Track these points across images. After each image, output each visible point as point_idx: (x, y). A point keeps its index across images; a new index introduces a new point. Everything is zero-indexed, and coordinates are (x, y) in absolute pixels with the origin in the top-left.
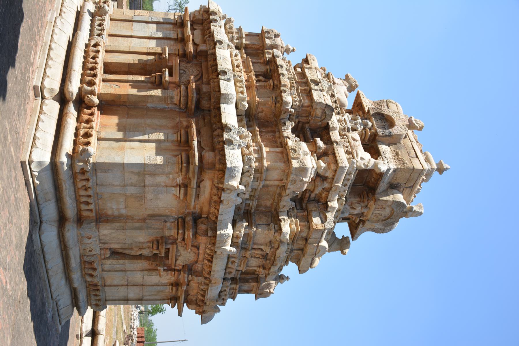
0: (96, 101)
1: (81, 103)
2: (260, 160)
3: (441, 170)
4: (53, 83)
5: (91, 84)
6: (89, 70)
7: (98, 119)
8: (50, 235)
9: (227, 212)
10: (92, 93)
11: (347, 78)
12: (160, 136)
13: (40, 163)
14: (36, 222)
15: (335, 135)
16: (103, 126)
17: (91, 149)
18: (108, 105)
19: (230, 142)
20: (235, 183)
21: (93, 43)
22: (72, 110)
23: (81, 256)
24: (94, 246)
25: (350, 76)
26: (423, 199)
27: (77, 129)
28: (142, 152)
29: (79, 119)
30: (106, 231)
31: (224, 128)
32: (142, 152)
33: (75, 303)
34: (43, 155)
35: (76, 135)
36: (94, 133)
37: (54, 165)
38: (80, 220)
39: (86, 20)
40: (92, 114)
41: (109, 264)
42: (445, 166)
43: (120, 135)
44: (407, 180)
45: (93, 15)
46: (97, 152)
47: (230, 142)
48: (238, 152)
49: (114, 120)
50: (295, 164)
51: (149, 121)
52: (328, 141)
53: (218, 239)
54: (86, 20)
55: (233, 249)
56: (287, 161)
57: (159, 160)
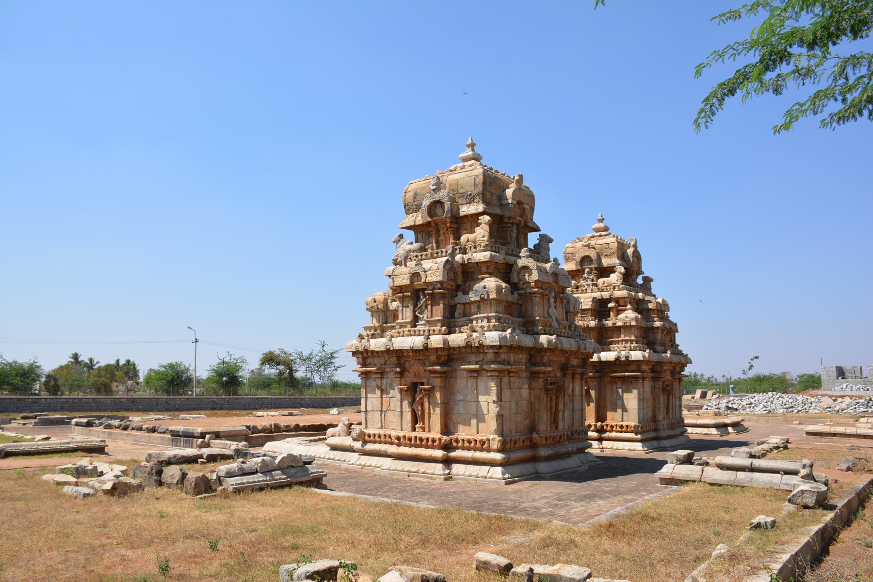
0: (599, 424)
1: (601, 431)
2: (632, 342)
3: (472, 146)
4: (439, 468)
5: (434, 441)
6: (422, 443)
7: (609, 422)
8: (543, 467)
9: (527, 341)
10: (596, 425)
11: (397, 242)
12: (620, 391)
13: (503, 474)
14: (538, 476)
15: (606, 295)
16: (613, 420)
17: (633, 424)
18: (446, 430)
19: (627, 357)
20: (647, 355)
21: (397, 441)
22: (607, 435)
23: (669, 429)
24: (665, 423)
25: (393, 239)
26: (507, 168)
27: (617, 432)
28: (631, 400)
29: (611, 431)
30: (661, 417)
31: (618, 359)
32: (631, 400)
33: (581, 450)
34: (497, 472)
35: (621, 432)
36: (620, 423)
37: (502, 464)
38: (656, 430)
39: (370, 447)
40: (607, 425)
41: (560, 427)
42: (470, 142)
43: (619, 411)
44: (491, 186)
45: (365, 442)
46: (632, 420)
47: (627, 357)
48: (632, 353)
49: (609, 414)
50: (633, 323)
51: (608, 397)
52: (609, 300)
53: (503, 344)
54: (370, 447)
55: (669, 352)
56: (631, 327)
57: (635, 392)
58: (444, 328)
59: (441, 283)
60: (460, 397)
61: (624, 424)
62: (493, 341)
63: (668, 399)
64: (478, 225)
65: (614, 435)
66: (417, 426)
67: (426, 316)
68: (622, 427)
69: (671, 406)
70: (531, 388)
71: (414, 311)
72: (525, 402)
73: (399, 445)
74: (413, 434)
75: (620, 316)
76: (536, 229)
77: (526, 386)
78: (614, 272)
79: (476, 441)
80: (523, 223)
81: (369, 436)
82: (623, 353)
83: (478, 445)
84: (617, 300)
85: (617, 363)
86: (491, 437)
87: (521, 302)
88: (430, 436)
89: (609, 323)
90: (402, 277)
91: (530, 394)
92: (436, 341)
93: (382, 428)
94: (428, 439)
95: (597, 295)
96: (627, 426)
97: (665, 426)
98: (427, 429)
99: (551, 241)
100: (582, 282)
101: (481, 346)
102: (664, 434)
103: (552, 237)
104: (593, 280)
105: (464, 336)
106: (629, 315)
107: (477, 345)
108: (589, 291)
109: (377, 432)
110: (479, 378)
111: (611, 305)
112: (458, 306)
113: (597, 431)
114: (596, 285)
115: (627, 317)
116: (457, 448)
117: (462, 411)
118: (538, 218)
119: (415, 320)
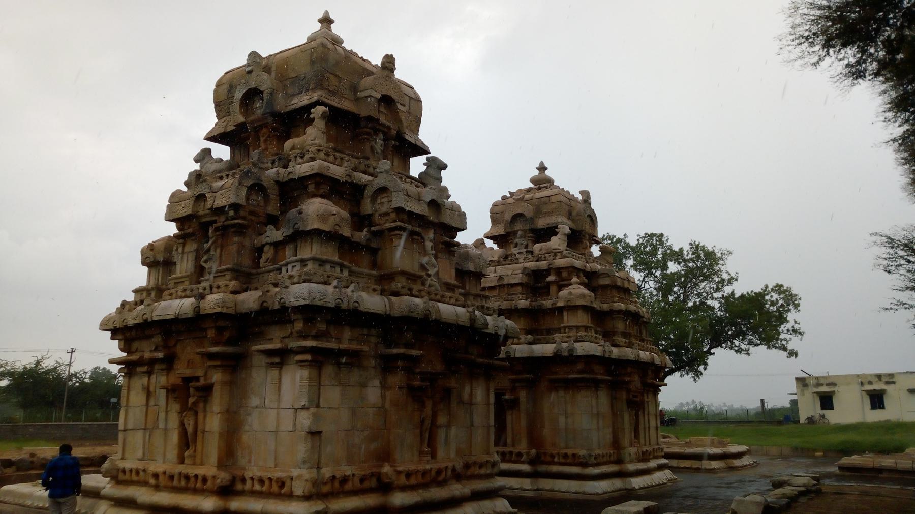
0: (534, 451)
15: (543, 265)
21: (152, 481)
41: (441, 453)
48: (577, 345)
52: (548, 272)
58: (234, 282)
59: (235, 207)
60: (254, 401)
61: (570, 452)
62: (299, 299)
63: (637, 416)
64: (311, 121)
65: (555, 468)
66: (186, 454)
67: (214, 266)
68: (566, 456)
69: (641, 427)
70: (384, 387)
71: (197, 259)
72: (371, 411)
73: (157, 488)
74: (181, 468)
75: (561, 293)
76: (421, 150)
77: (377, 383)
78: (556, 234)
79: (270, 479)
80: (394, 132)
81: (124, 471)
82: (565, 345)
83: (275, 488)
84: (558, 271)
85: (557, 358)
86: (295, 473)
87: (374, 245)
88: (201, 471)
89: (547, 303)
90: (183, 204)
91: (383, 397)
92: (213, 301)
93: (142, 459)
94: (196, 476)
95: (532, 265)
96: (574, 455)
97: (633, 456)
98: (198, 460)
99: (444, 167)
100: (515, 251)
101: (284, 309)
102: (631, 467)
103: (444, 159)
104: (526, 247)
105: (258, 293)
106: (576, 291)
107: (277, 306)
108: (521, 261)
109: (140, 465)
110: (284, 368)
111: (551, 278)
112: (266, 248)
113: (531, 462)
114: (532, 252)
115: (570, 293)
116: (241, 493)
117: (256, 426)
118: (426, 134)
119: (200, 271)
